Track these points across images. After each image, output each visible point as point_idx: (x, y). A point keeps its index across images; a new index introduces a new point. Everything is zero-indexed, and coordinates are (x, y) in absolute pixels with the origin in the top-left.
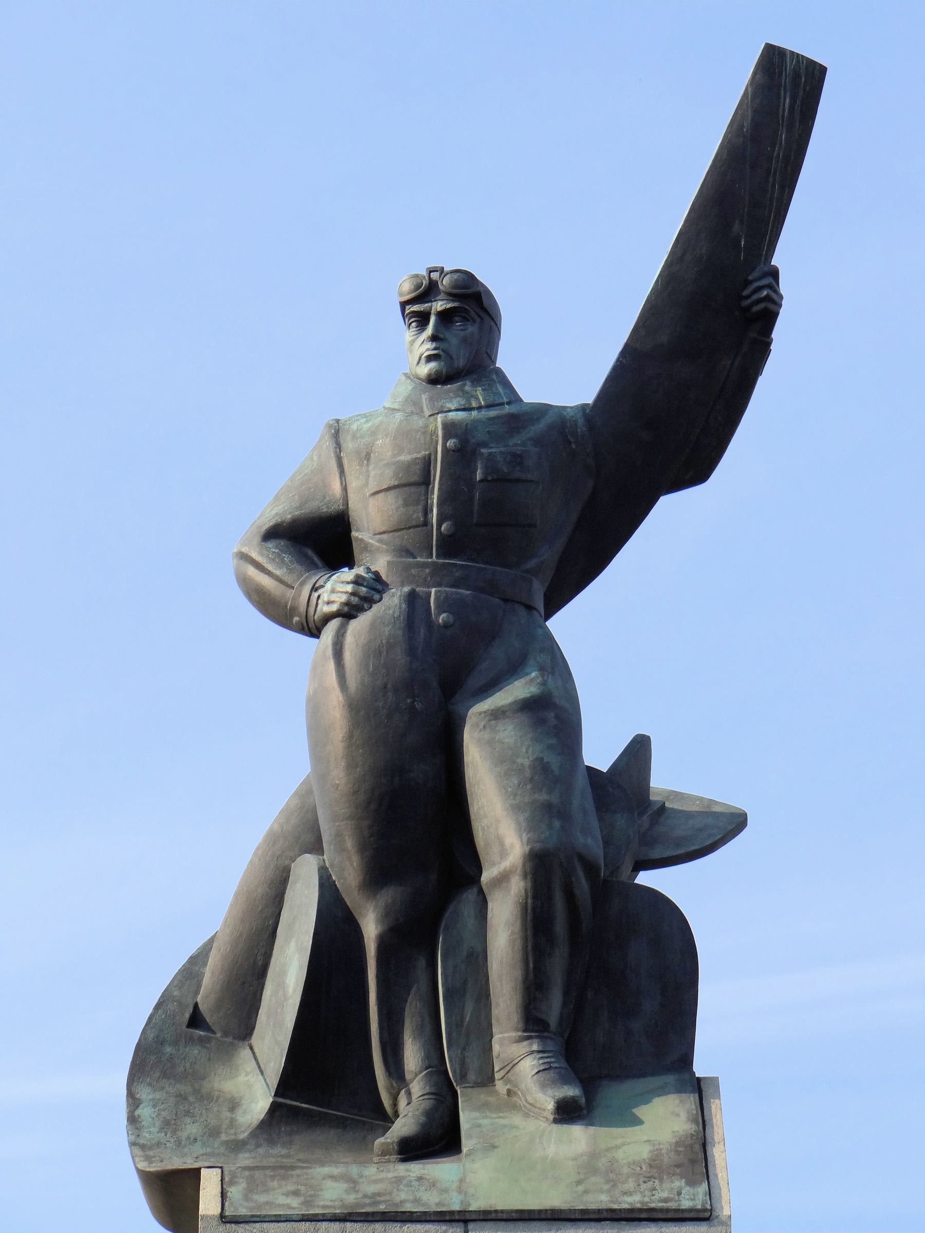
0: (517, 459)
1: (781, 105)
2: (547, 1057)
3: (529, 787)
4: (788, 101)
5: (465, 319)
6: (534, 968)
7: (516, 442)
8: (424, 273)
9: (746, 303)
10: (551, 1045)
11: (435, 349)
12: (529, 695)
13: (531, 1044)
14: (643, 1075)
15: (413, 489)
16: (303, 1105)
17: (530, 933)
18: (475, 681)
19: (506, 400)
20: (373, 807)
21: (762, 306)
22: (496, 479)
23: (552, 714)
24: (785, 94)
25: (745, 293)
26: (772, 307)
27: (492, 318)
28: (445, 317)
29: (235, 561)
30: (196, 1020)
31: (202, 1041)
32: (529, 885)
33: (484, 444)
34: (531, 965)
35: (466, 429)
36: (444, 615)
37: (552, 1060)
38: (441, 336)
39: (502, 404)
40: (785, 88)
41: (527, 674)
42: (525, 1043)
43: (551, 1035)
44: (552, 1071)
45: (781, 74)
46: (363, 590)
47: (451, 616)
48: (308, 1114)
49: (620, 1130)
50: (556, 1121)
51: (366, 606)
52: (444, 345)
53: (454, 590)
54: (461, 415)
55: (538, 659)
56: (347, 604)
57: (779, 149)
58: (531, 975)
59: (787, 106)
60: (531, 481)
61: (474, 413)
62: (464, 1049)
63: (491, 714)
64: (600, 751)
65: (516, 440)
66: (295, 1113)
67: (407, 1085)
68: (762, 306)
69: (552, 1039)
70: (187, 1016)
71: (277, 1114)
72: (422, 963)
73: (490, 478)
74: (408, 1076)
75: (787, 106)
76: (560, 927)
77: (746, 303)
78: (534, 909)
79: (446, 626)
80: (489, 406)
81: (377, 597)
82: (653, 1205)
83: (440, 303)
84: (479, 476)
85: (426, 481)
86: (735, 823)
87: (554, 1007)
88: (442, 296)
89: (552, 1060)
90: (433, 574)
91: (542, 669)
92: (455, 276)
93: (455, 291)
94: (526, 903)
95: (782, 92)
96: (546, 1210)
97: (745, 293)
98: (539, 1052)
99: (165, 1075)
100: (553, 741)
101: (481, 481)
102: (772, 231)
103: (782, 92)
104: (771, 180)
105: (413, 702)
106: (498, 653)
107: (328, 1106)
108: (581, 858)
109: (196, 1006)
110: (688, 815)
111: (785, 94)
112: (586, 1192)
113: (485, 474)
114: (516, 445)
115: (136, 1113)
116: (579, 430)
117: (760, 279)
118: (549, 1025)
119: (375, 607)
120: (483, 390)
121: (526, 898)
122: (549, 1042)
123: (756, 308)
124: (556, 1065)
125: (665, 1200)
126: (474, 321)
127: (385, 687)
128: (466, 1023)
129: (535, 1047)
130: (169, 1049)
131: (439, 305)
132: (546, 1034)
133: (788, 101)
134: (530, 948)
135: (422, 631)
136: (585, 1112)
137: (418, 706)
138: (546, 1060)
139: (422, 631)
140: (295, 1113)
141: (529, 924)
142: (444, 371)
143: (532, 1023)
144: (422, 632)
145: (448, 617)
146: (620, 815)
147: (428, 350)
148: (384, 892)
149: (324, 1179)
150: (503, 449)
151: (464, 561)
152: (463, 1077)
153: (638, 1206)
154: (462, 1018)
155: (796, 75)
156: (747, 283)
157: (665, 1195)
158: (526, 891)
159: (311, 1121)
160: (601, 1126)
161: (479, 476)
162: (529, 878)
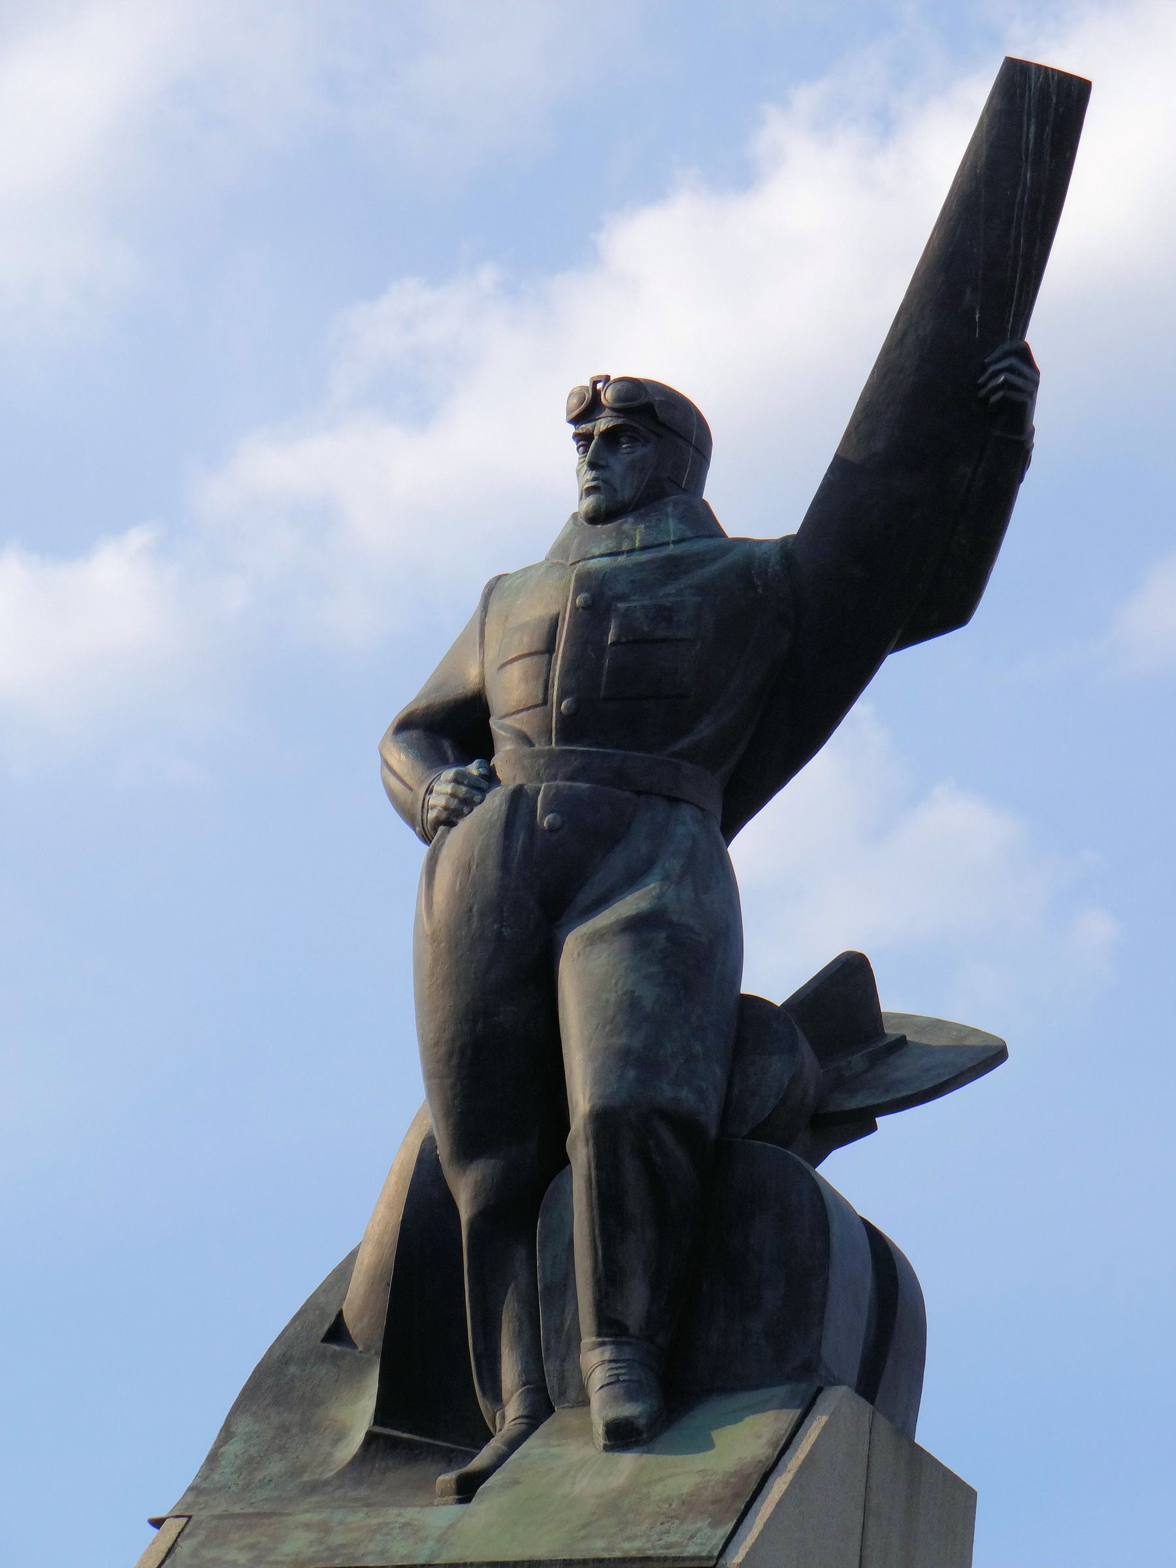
0: (664, 614)
1: (1024, 135)
2: (617, 1368)
3: (607, 1028)
4: (1032, 128)
5: (633, 440)
6: (604, 1256)
7: (668, 593)
8: (588, 384)
9: (983, 392)
10: (628, 1353)
11: (594, 479)
12: (634, 912)
13: (603, 1353)
14: (758, 1386)
15: (535, 658)
16: (405, 1435)
17: (596, 1212)
18: (585, 897)
19: (672, 538)
20: (454, 1062)
21: (1000, 394)
22: (632, 641)
23: (663, 935)
24: (1029, 119)
25: (982, 380)
26: (1018, 397)
27: (680, 436)
28: (610, 437)
29: (400, 759)
30: (337, 1332)
31: (335, 1357)
32: (592, 1152)
33: (624, 598)
34: (600, 1253)
35: (603, 580)
36: (550, 816)
37: (623, 1371)
38: (603, 463)
39: (667, 544)
40: (1029, 114)
41: (647, 885)
42: (598, 1351)
43: (633, 1340)
44: (618, 1386)
45: (1022, 97)
46: (463, 790)
47: (559, 817)
48: (409, 1445)
49: (678, 1459)
50: (607, 1448)
51: (465, 810)
52: (606, 474)
53: (569, 783)
54: (605, 561)
55: (667, 865)
56: (446, 808)
57: (1024, 192)
58: (601, 1266)
59: (1031, 135)
60: (682, 640)
61: (621, 559)
62: (563, 1360)
63: (588, 939)
64: (774, 969)
65: (671, 589)
66: (393, 1444)
67: (503, 1407)
68: (1000, 394)
69: (630, 1344)
70: (326, 1327)
71: (373, 1446)
72: (521, 1253)
73: (624, 640)
74: (505, 1396)
75: (1031, 135)
76: (636, 1201)
77: (983, 392)
78: (598, 1182)
79: (552, 829)
80: (644, 548)
81: (477, 798)
82: (650, 1553)
83: (603, 421)
84: (611, 639)
85: (549, 648)
86: (992, 1056)
87: (636, 1302)
88: (607, 412)
89: (623, 1371)
90: (547, 766)
91: (665, 878)
92: (623, 383)
93: (617, 405)
94: (590, 1175)
95: (1025, 118)
96: (523, 1562)
97: (982, 380)
98: (610, 1361)
99: (276, 1402)
100: (655, 969)
101: (613, 644)
102: (1019, 297)
103: (1025, 118)
104: (1013, 232)
105: (499, 929)
106: (618, 860)
107: (434, 1436)
108: (664, 1115)
109: (340, 1315)
110: (927, 1050)
111: (1029, 119)
112: (584, 1538)
113: (619, 636)
114: (669, 595)
115: (222, 1450)
116: (770, 570)
117: (1000, 359)
118: (627, 1328)
119: (476, 810)
120: (646, 528)
121: (589, 1168)
122: (627, 1349)
123: (994, 399)
124: (626, 1377)
125: (668, 1547)
126: (647, 441)
127: (471, 910)
128: (566, 1328)
129: (607, 1356)
130: (293, 1369)
131: (602, 424)
132: (624, 1339)
133: (1032, 128)
134: (597, 1231)
135: (521, 837)
136: (645, 1436)
137: (506, 932)
138: (615, 1372)
139: (521, 837)
140: (393, 1444)
141: (595, 1201)
142: (603, 506)
143: (609, 1326)
144: (521, 839)
145: (554, 819)
146: (777, 1057)
147: (587, 481)
148: (474, 1165)
149: (297, 1528)
150: (646, 603)
151: (588, 746)
152: (562, 1393)
153: (633, 1554)
154: (562, 1323)
155: (1044, 94)
156: (984, 368)
157: (673, 1538)
158: (589, 1159)
159: (409, 1453)
160: (660, 1453)
161: (611, 639)
162: (591, 1144)
